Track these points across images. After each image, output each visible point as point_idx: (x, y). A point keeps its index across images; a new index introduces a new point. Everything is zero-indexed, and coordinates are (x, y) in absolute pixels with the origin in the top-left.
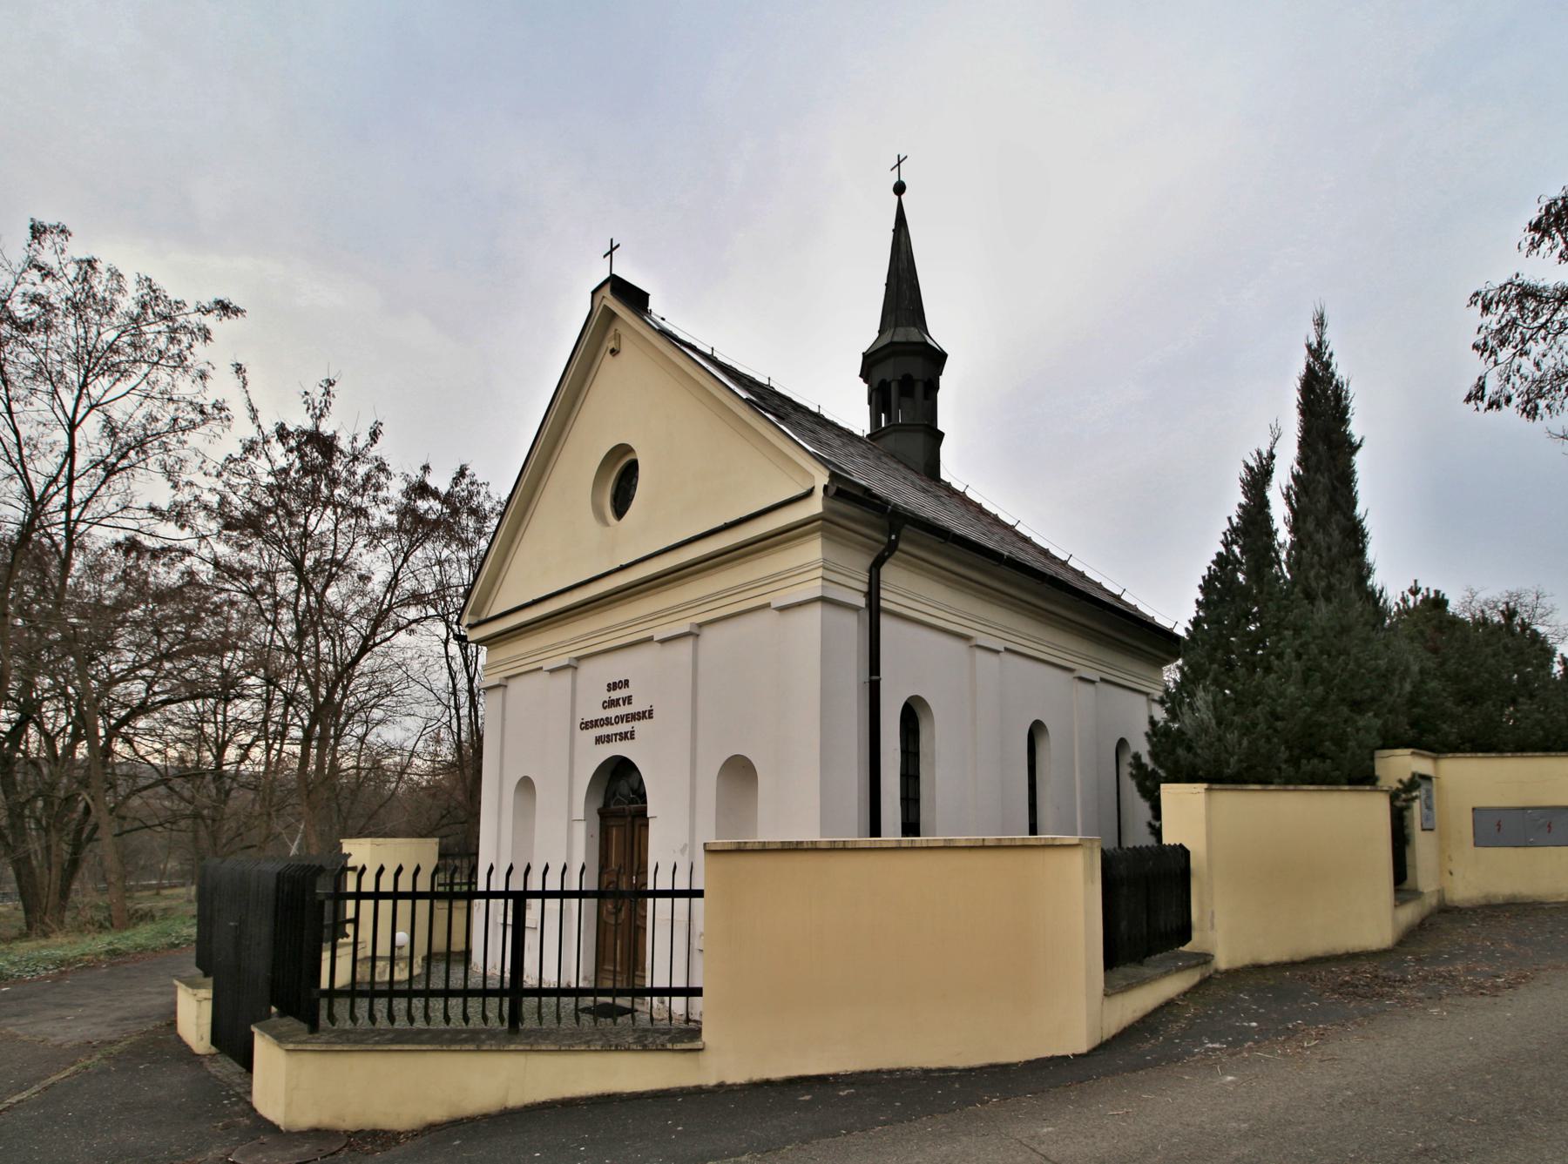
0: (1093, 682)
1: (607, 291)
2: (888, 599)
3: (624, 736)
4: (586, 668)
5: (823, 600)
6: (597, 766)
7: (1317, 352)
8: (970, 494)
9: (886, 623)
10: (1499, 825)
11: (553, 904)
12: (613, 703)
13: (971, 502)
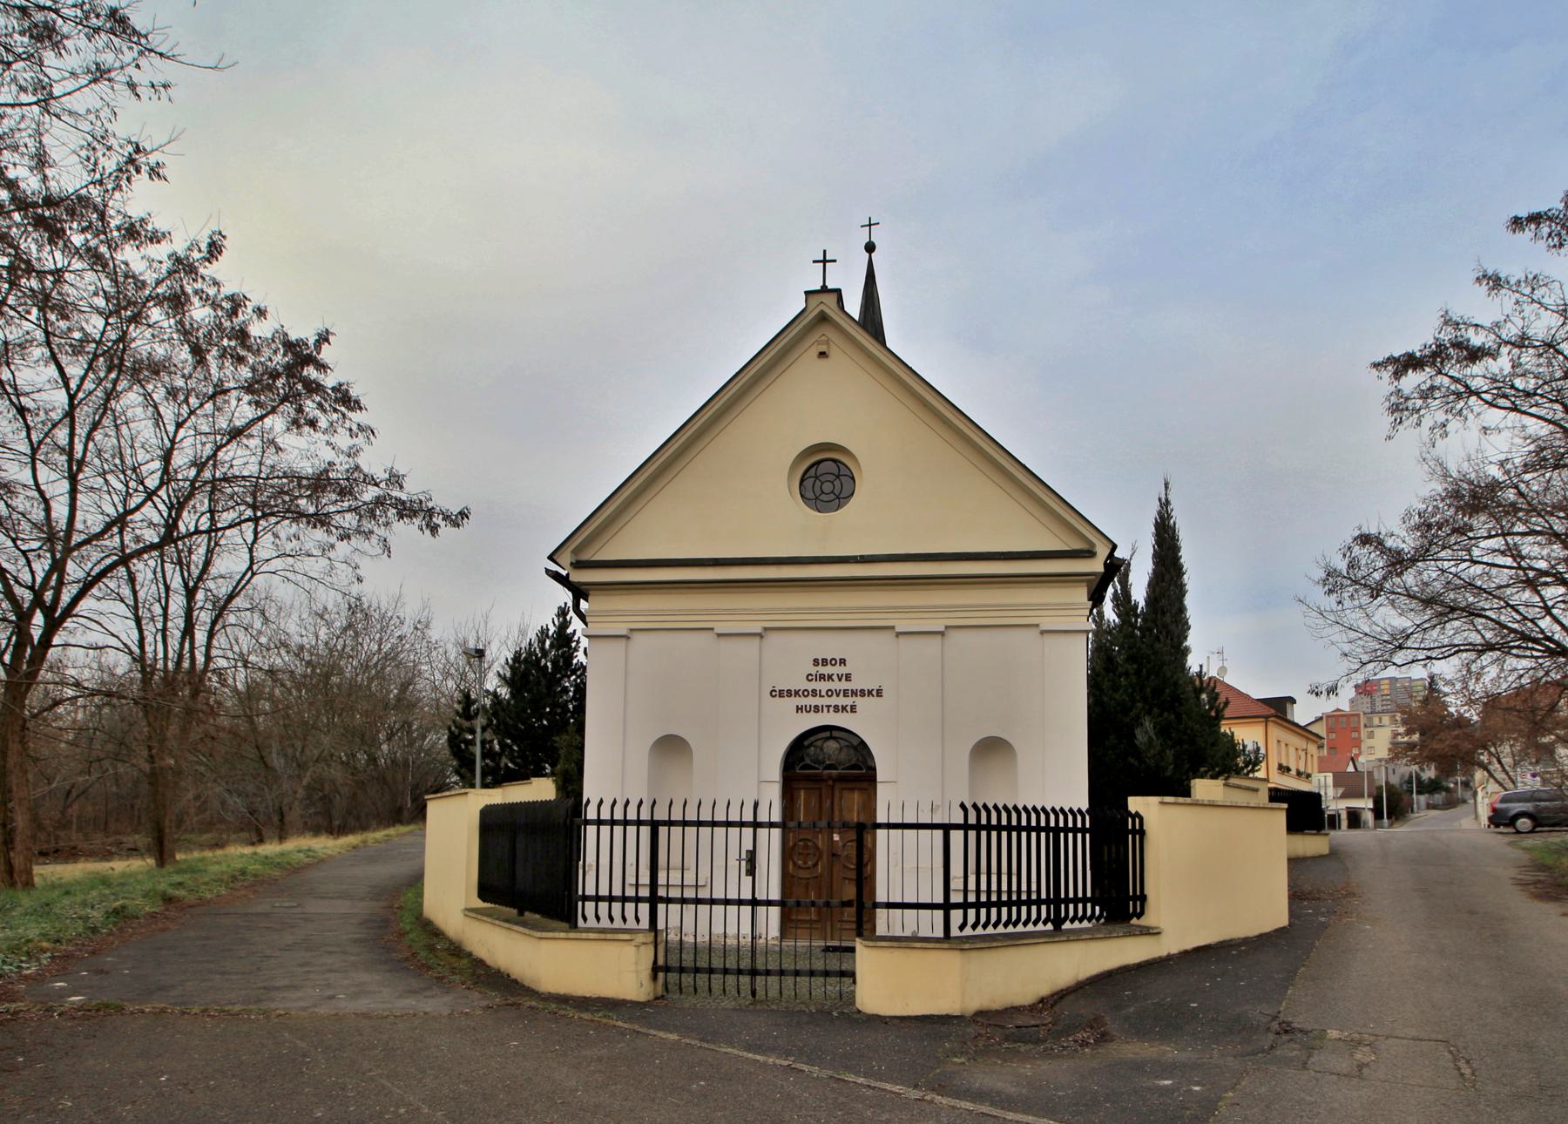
6: (980, 738)
7: (1165, 504)
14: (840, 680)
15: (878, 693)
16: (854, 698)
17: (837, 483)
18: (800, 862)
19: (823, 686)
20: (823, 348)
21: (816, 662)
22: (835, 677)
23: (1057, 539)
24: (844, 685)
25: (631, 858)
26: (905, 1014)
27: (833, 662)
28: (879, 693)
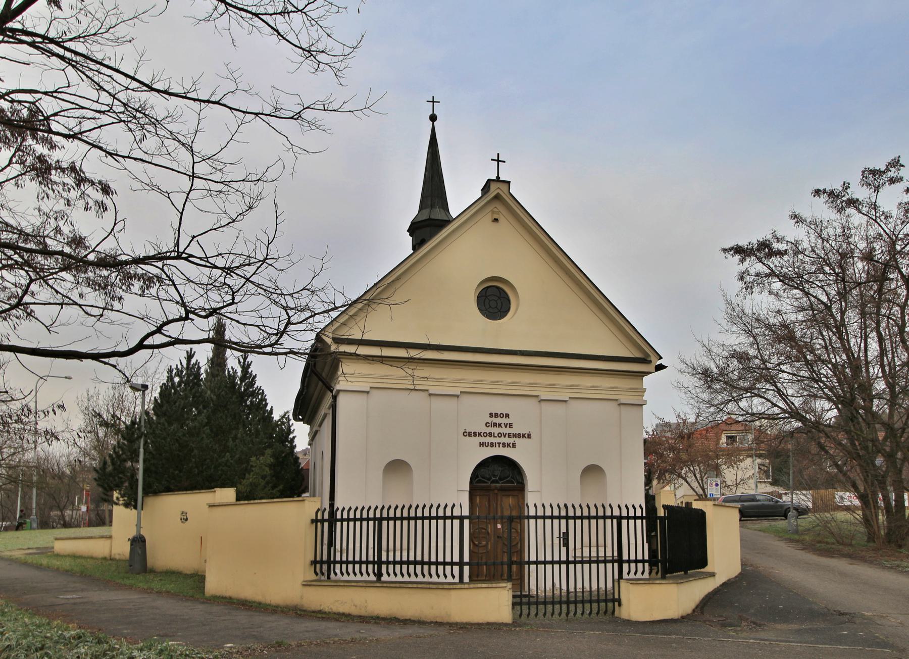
14: (506, 427)
15: (528, 436)
16: (515, 439)
17: (499, 301)
18: (476, 543)
19: (496, 430)
20: (496, 216)
21: (491, 415)
22: (503, 425)
23: (628, 351)
24: (508, 430)
25: (540, 538)
26: (651, 620)
27: (502, 415)
28: (529, 436)
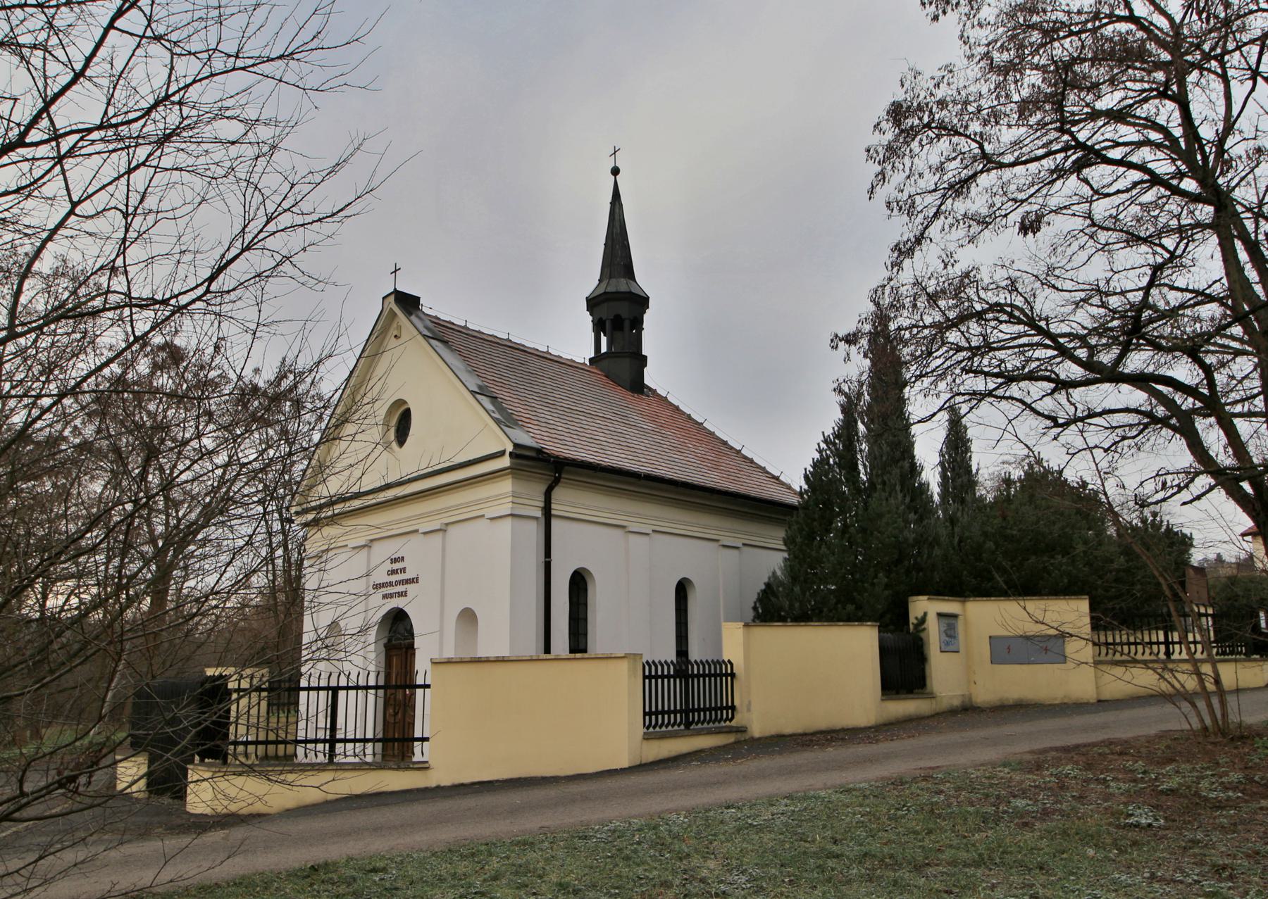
0: (737, 548)
1: (392, 298)
2: (556, 508)
3: (401, 594)
4: (377, 547)
5: (512, 515)
8: (670, 399)
9: (554, 522)
10: (1009, 648)
11: (352, 693)
12: (394, 572)
13: (671, 404)
